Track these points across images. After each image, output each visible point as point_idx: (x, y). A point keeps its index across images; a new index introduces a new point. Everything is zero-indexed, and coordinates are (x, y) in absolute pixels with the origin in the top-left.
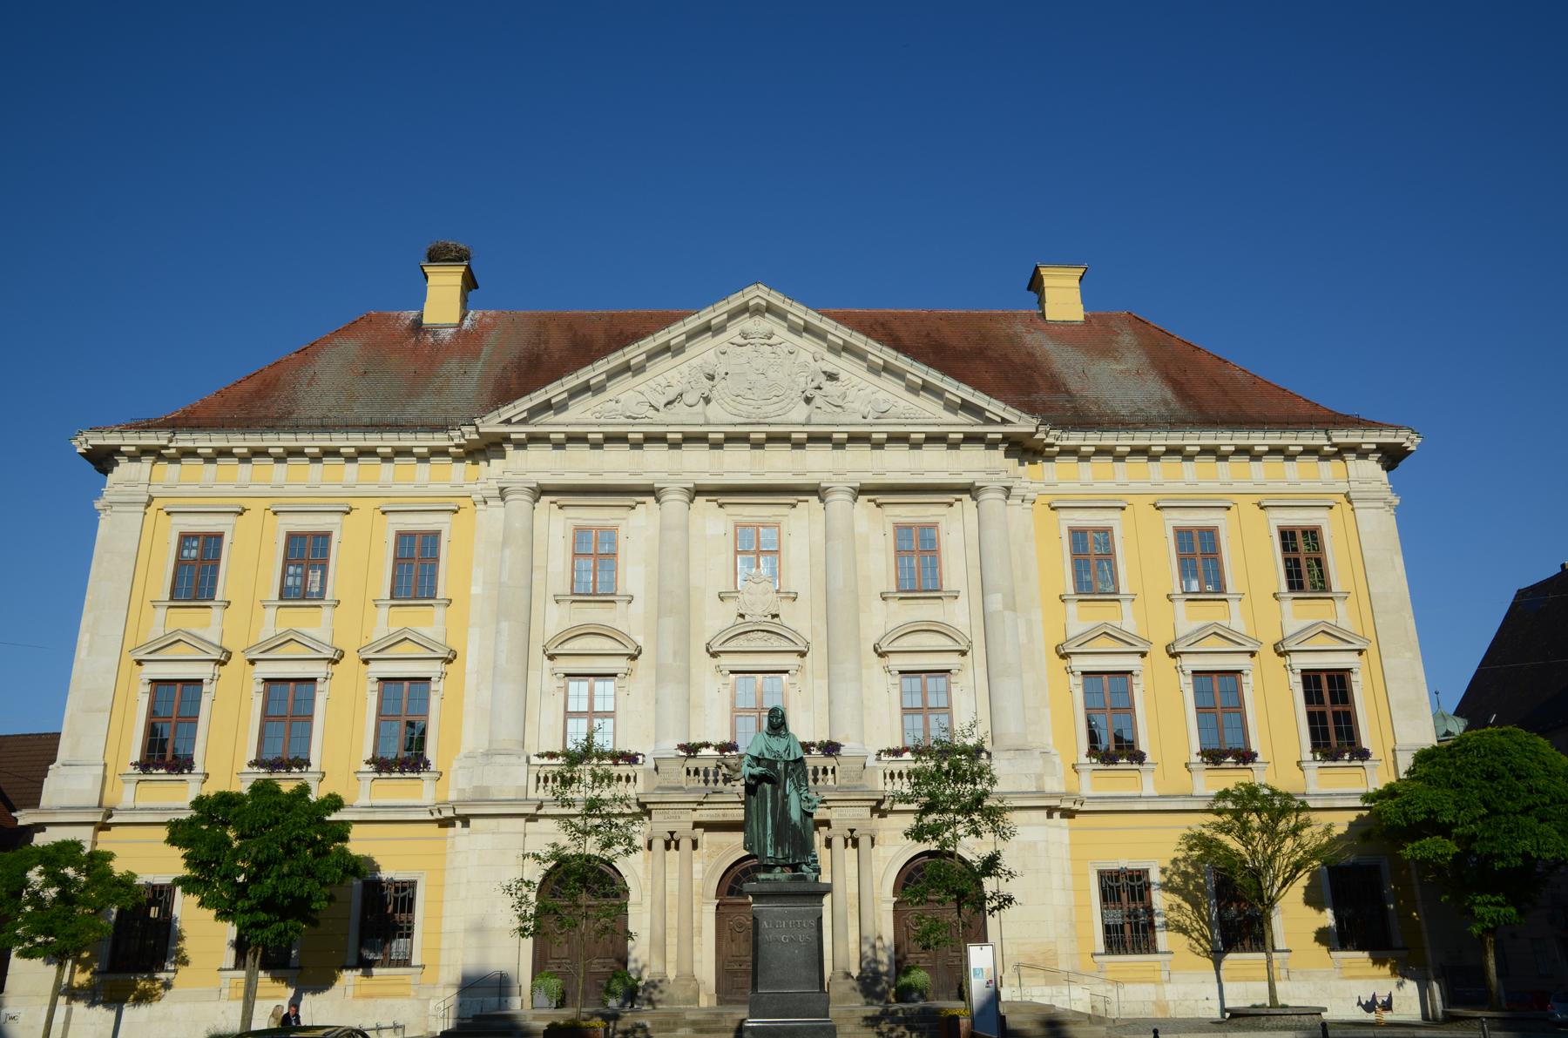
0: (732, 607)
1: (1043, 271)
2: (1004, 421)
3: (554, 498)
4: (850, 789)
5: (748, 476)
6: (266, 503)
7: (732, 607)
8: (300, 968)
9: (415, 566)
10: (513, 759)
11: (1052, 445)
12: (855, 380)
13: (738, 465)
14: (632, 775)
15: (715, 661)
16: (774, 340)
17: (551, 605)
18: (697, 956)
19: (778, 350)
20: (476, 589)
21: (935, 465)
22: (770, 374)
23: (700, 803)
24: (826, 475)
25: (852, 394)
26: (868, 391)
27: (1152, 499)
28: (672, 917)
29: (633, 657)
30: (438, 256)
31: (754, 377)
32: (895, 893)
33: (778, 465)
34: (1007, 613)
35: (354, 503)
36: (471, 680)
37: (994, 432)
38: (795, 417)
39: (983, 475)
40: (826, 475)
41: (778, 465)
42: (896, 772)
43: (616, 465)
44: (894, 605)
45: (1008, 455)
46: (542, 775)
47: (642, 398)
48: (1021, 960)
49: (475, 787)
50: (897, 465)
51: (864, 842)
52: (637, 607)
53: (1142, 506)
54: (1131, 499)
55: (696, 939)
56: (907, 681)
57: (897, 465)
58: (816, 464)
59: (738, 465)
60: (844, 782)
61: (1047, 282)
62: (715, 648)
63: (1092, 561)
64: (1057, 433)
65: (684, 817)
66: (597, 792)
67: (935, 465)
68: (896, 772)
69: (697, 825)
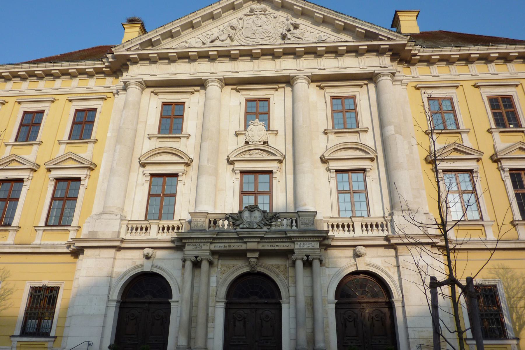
0: (242, 139)
1: (399, 14)
2: (389, 39)
3: (152, 89)
4: (305, 231)
5: (252, 73)
6: (15, 99)
7: (242, 139)
8: (56, 337)
9: (83, 124)
10: (113, 217)
11: (415, 55)
12: (308, 28)
13: (246, 68)
14: (148, 226)
15: (232, 167)
16: (267, 12)
17: (147, 141)
18: (210, 335)
19: (269, 17)
20: (109, 135)
21: (351, 64)
22: (264, 26)
23: (214, 238)
24: (294, 71)
25: (307, 34)
26: (316, 33)
27: (473, 83)
28: (200, 308)
29: (187, 165)
30: (131, 21)
31: (255, 28)
32: (336, 297)
33: (266, 68)
34: (397, 135)
35: (57, 97)
36: (100, 178)
37: (384, 44)
38: (278, 45)
39: (379, 68)
40: (294, 71)
41: (266, 68)
42: (335, 224)
43: (182, 70)
44: (331, 136)
45: (392, 60)
46: (130, 226)
47: (198, 40)
48: (421, 342)
49: (90, 232)
50: (330, 65)
51: (316, 263)
52: (192, 140)
53: (468, 86)
54: (462, 83)
55: (210, 324)
56: (340, 175)
57: (330, 65)
58: (286, 66)
59: (246, 68)
60: (303, 227)
61: (401, 18)
62: (232, 158)
63: (441, 114)
64: (418, 48)
65: (204, 247)
66: (31, 175)
67: (351, 64)
68: (335, 224)
69: (214, 253)
